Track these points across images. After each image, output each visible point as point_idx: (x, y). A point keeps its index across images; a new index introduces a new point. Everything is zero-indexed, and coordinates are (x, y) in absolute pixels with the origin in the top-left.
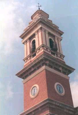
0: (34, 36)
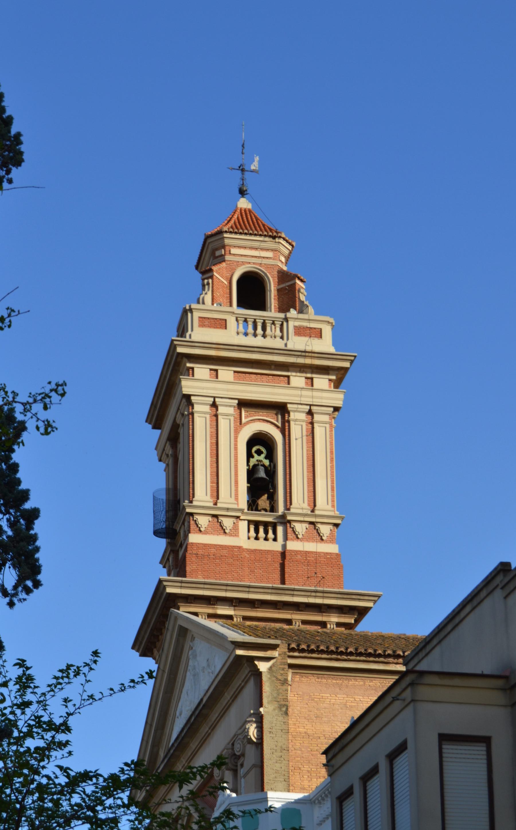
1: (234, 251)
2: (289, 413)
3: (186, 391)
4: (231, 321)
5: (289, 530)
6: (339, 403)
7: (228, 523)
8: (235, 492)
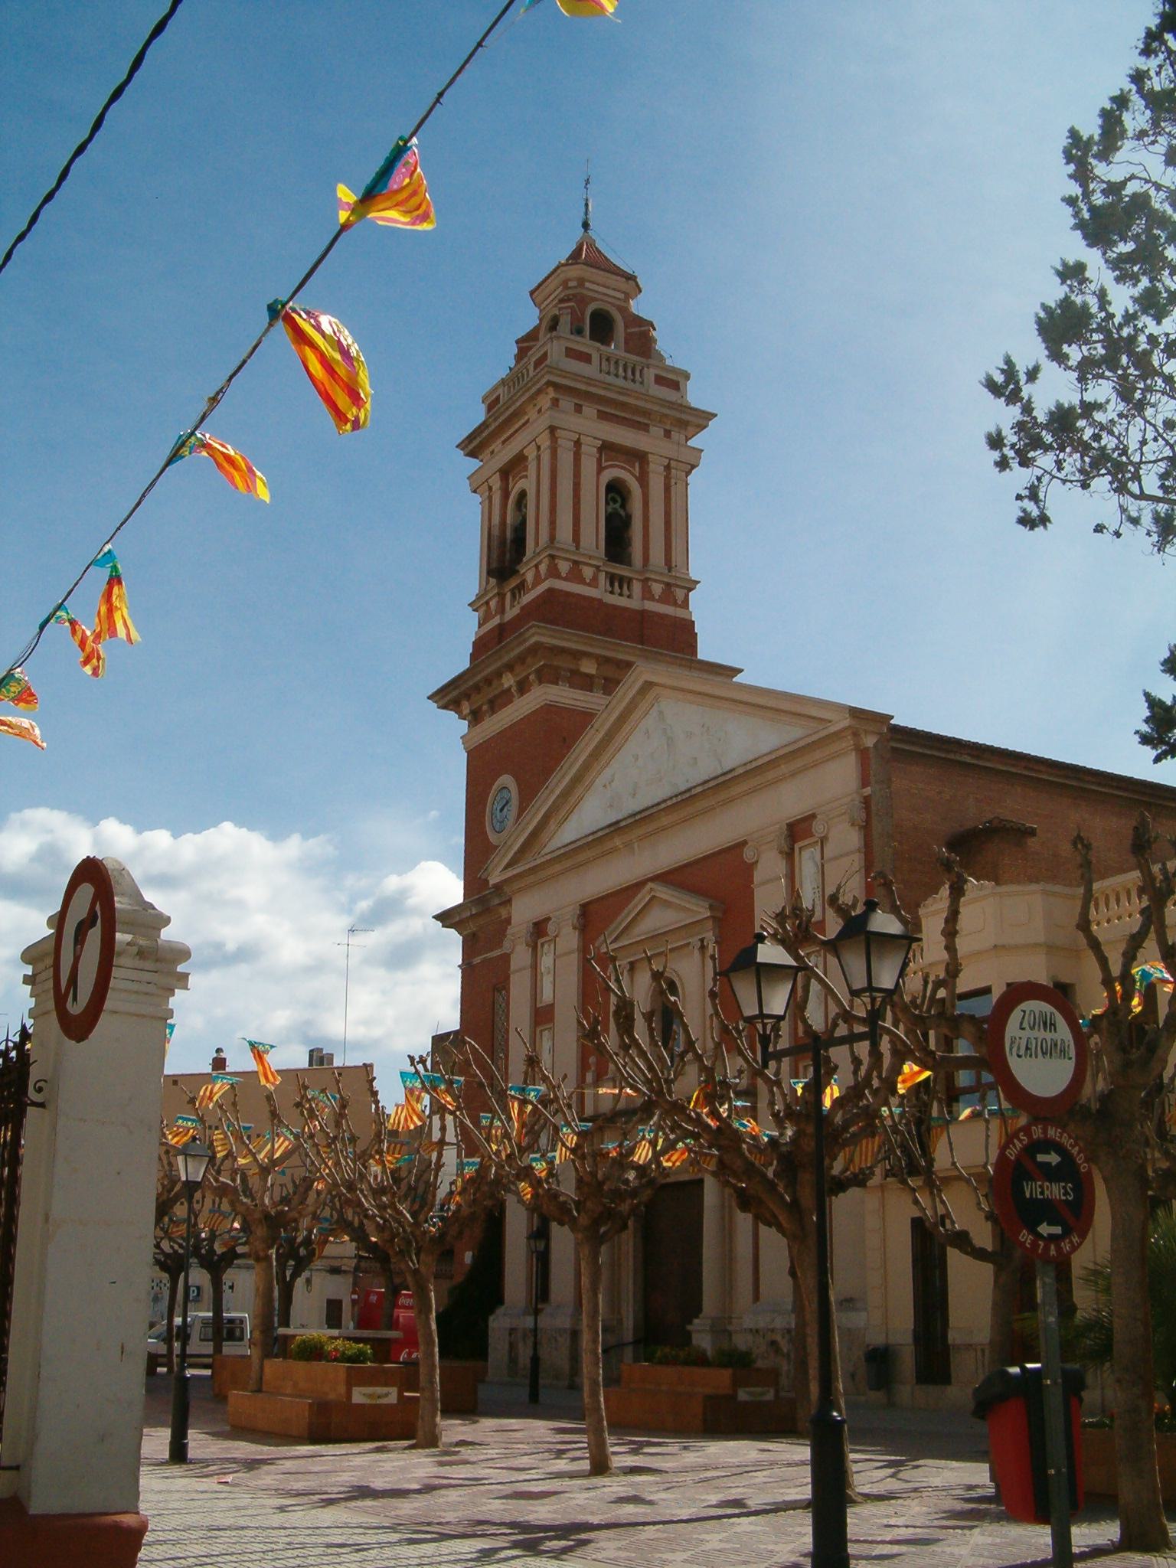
0: (540, 562)
4: (595, 357)
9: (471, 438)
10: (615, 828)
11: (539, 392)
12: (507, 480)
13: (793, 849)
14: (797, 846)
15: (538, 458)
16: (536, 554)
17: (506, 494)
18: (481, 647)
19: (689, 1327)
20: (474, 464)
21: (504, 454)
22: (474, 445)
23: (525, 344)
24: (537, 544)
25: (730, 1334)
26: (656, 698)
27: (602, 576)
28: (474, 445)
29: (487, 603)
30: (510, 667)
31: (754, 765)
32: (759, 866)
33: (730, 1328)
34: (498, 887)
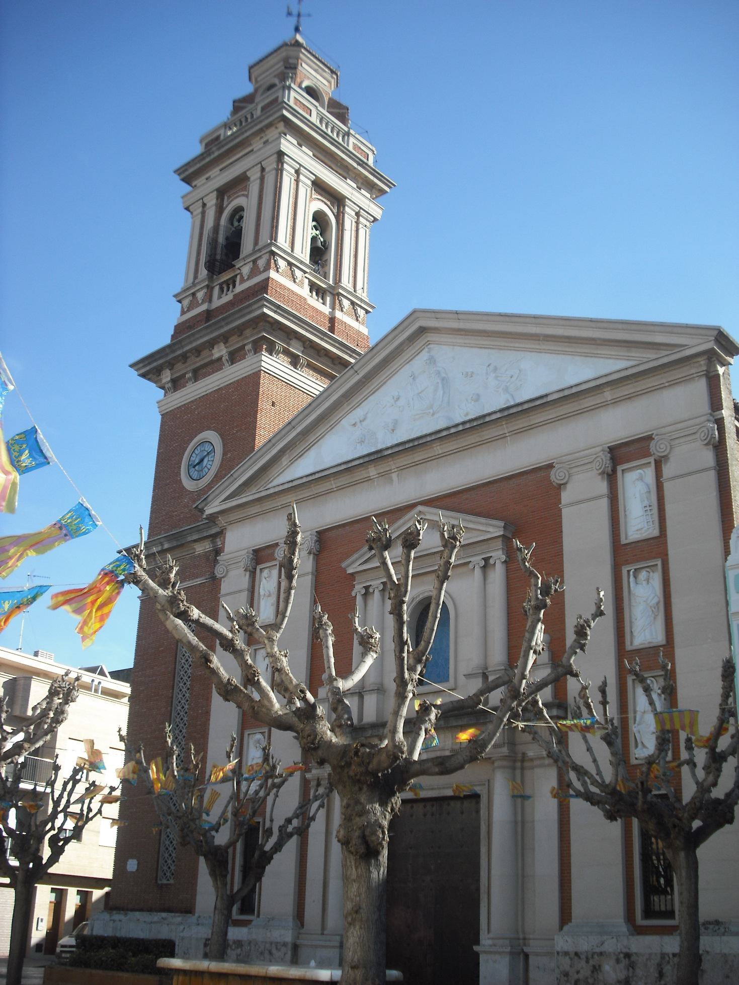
0: (260, 257)
1: (304, 65)
2: (344, 207)
3: (283, 148)
4: (314, 112)
5: (337, 302)
6: (378, 217)
7: (298, 273)
8: (303, 253)
9: (188, 165)
10: (377, 457)
11: (270, 125)
12: (222, 200)
13: (614, 471)
14: (619, 469)
15: (262, 179)
16: (254, 252)
17: (220, 210)
18: (180, 329)
19: (476, 948)
20: (187, 188)
21: (219, 177)
22: (190, 174)
23: (239, 105)
24: (256, 242)
25: (526, 956)
26: (428, 343)
27: (306, 281)
28: (190, 174)
29: (194, 294)
30: (225, 338)
31: (574, 390)
32: (569, 486)
33: (526, 949)
34: (213, 518)
